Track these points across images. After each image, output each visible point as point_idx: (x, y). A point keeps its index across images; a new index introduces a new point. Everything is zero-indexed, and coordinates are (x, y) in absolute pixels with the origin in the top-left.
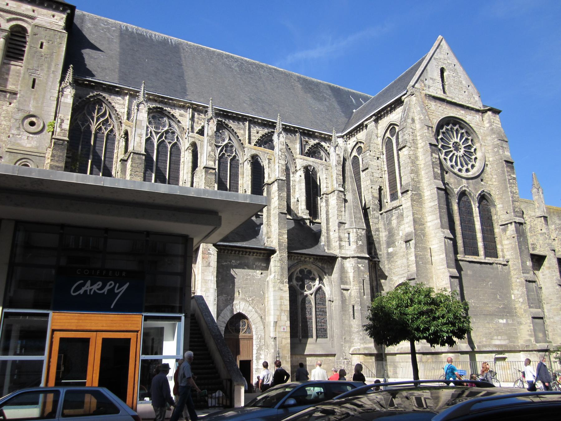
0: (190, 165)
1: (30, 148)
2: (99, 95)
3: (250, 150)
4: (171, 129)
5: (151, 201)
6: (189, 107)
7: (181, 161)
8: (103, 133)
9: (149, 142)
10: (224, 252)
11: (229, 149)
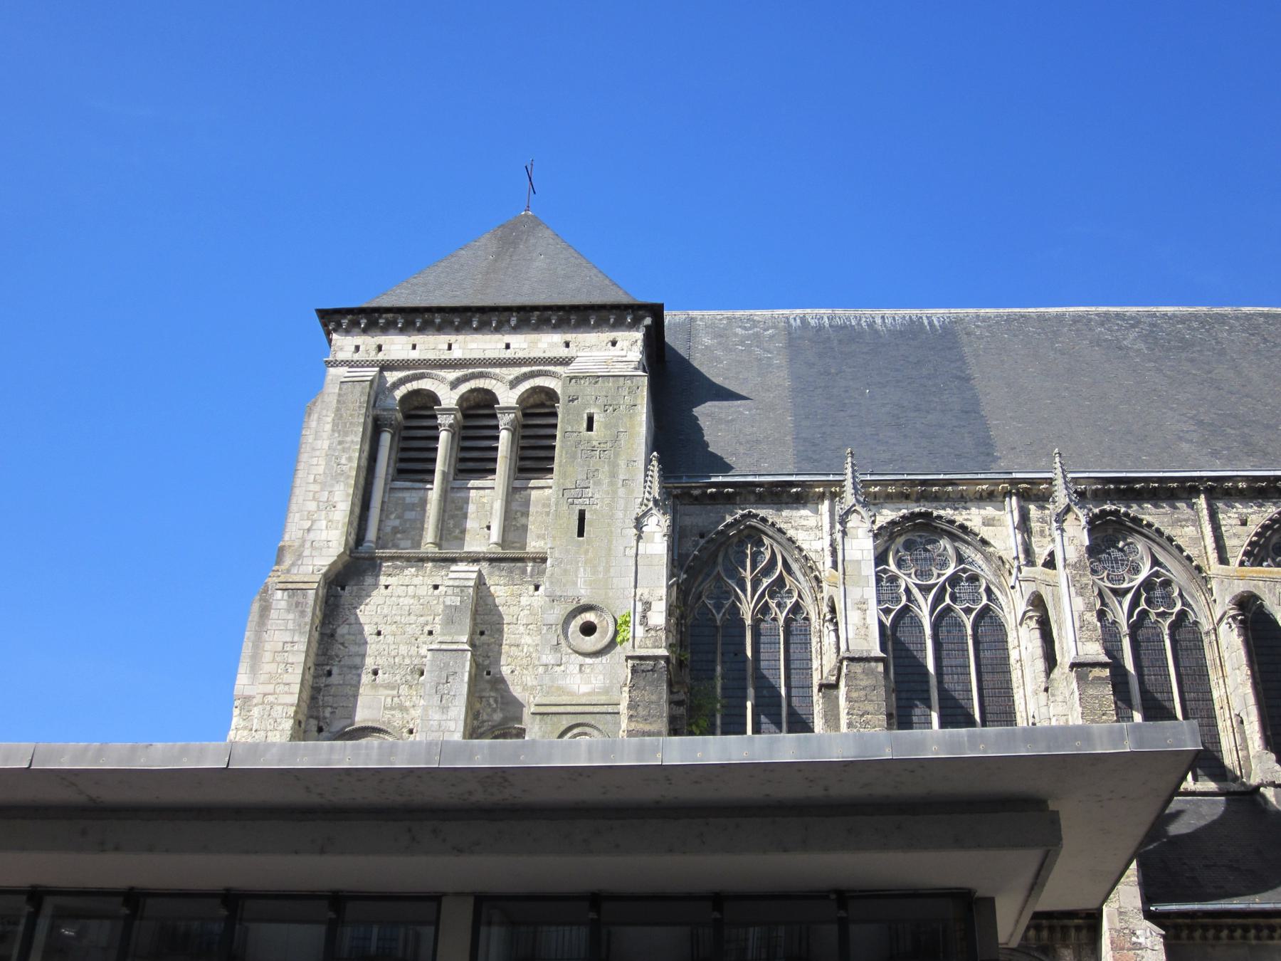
0: (1040, 665)
1: (589, 694)
2: (750, 516)
3: (1228, 582)
4: (964, 570)
5: (816, 792)
6: (1008, 494)
7: (1012, 661)
8: (775, 619)
9: (907, 620)
10: (1190, 938)
11: (1158, 593)
